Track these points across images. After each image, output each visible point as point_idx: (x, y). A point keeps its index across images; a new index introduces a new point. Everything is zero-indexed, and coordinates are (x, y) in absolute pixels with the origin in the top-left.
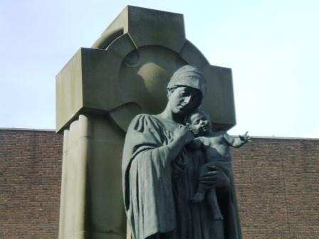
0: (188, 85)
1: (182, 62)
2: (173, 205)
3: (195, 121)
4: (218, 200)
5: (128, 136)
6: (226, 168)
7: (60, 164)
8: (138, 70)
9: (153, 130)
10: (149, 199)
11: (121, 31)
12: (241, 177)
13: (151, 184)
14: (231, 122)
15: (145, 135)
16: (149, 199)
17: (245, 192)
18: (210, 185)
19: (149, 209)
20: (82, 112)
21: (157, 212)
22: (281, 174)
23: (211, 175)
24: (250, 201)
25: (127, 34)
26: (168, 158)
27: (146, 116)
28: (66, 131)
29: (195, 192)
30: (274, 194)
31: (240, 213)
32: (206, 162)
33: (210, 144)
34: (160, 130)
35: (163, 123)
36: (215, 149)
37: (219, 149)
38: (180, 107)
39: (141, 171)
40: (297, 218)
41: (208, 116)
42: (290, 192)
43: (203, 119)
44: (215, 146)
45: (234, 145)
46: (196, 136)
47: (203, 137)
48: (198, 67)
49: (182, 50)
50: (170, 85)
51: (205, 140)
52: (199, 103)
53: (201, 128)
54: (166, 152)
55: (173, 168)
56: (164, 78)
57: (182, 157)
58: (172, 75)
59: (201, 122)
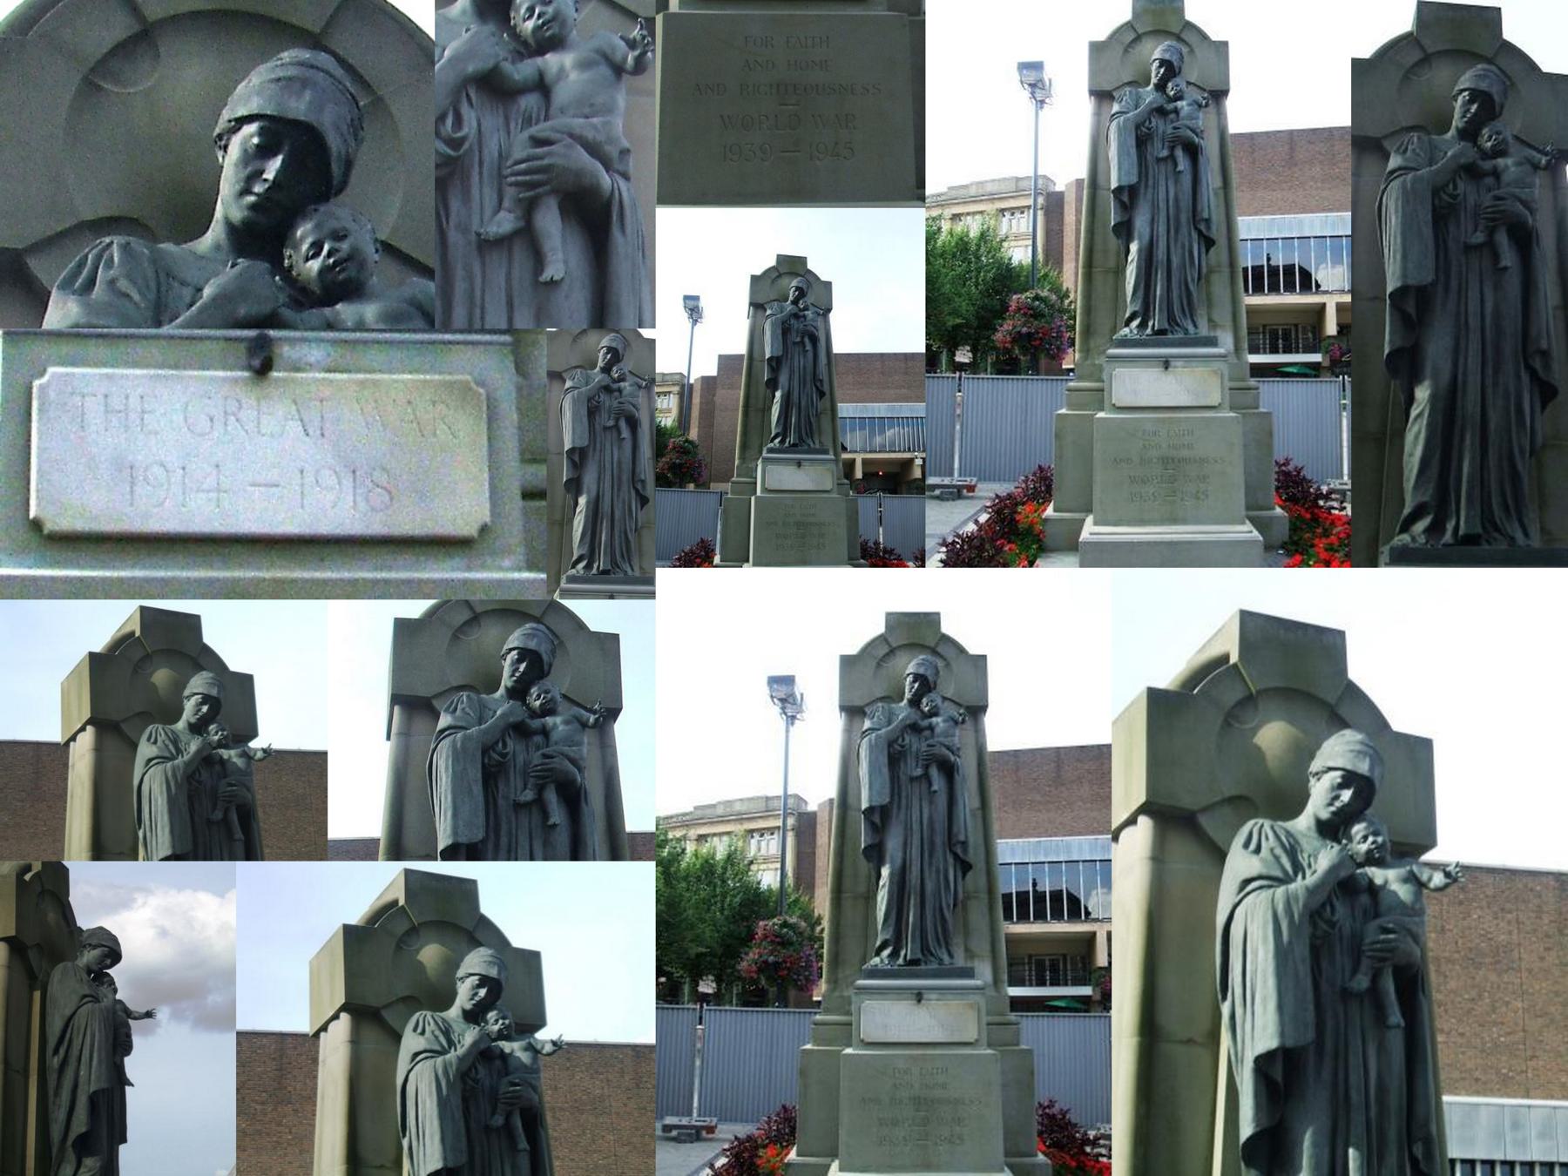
0: (1349, 767)
1: (1339, 722)
2: (463, 1131)
3: (1358, 837)
4: (1397, 991)
5: (404, 1040)
6: (1414, 928)
7: (316, 1077)
8: (1254, 735)
9: (437, 1033)
10: (1265, 982)
11: (1225, 658)
12: (553, 1095)
13: (1271, 955)
14: (540, 1023)
15: (1263, 861)
16: (1265, 982)
17: (1444, 968)
18: (1383, 960)
19: (1264, 999)
20: (343, 1008)
21: (443, 1140)
22: (1515, 937)
23: (1383, 941)
24: (565, 1125)
25: (1235, 665)
26: (1305, 906)
27: (429, 1014)
28: (322, 1034)
29: (493, 1114)
30: (1499, 975)
31: (552, 1142)
32: (1377, 915)
33: (1386, 882)
34: (1292, 851)
35: (1299, 837)
36: (1395, 893)
37: (525, 1057)
38: (1333, 809)
39: (421, 1084)
40: (626, 1149)
41: (1384, 829)
42: (1530, 971)
43: (1376, 834)
44: (519, 1054)
45: (1432, 885)
46: (1361, 865)
47: (1373, 869)
48: (1368, 734)
49: (1340, 698)
50: (1315, 766)
51: (507, 1046)
52: (498, 997)
53: (1369, 852)
54: (1301, 894)
55: (1314, 925)
56: (1304, 752)
57: (1332, 907)
58: (1319, 746)
59: (1371, 839)
